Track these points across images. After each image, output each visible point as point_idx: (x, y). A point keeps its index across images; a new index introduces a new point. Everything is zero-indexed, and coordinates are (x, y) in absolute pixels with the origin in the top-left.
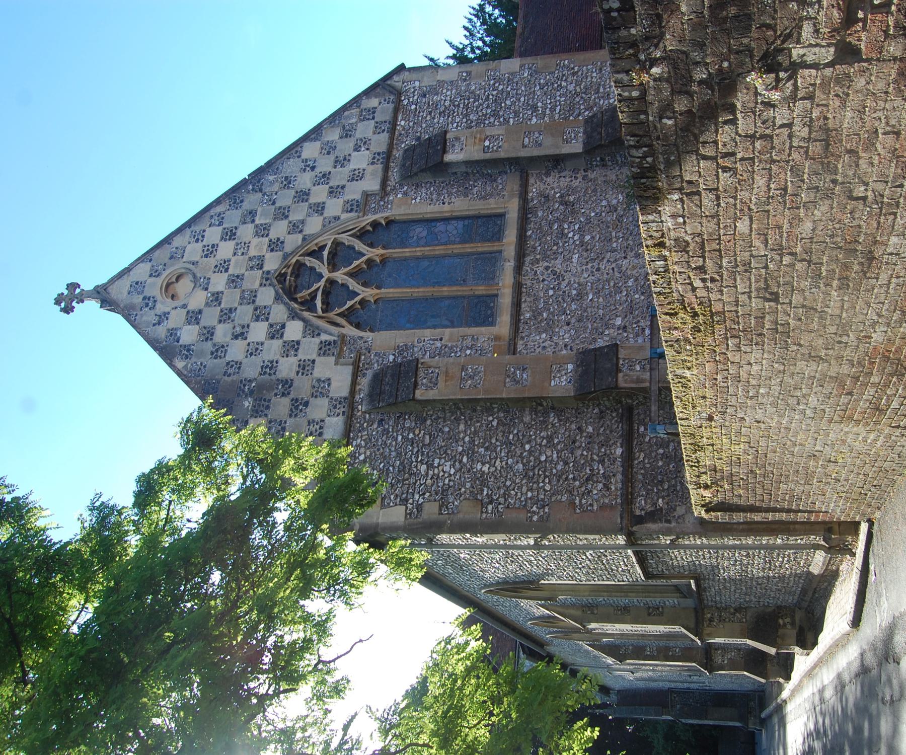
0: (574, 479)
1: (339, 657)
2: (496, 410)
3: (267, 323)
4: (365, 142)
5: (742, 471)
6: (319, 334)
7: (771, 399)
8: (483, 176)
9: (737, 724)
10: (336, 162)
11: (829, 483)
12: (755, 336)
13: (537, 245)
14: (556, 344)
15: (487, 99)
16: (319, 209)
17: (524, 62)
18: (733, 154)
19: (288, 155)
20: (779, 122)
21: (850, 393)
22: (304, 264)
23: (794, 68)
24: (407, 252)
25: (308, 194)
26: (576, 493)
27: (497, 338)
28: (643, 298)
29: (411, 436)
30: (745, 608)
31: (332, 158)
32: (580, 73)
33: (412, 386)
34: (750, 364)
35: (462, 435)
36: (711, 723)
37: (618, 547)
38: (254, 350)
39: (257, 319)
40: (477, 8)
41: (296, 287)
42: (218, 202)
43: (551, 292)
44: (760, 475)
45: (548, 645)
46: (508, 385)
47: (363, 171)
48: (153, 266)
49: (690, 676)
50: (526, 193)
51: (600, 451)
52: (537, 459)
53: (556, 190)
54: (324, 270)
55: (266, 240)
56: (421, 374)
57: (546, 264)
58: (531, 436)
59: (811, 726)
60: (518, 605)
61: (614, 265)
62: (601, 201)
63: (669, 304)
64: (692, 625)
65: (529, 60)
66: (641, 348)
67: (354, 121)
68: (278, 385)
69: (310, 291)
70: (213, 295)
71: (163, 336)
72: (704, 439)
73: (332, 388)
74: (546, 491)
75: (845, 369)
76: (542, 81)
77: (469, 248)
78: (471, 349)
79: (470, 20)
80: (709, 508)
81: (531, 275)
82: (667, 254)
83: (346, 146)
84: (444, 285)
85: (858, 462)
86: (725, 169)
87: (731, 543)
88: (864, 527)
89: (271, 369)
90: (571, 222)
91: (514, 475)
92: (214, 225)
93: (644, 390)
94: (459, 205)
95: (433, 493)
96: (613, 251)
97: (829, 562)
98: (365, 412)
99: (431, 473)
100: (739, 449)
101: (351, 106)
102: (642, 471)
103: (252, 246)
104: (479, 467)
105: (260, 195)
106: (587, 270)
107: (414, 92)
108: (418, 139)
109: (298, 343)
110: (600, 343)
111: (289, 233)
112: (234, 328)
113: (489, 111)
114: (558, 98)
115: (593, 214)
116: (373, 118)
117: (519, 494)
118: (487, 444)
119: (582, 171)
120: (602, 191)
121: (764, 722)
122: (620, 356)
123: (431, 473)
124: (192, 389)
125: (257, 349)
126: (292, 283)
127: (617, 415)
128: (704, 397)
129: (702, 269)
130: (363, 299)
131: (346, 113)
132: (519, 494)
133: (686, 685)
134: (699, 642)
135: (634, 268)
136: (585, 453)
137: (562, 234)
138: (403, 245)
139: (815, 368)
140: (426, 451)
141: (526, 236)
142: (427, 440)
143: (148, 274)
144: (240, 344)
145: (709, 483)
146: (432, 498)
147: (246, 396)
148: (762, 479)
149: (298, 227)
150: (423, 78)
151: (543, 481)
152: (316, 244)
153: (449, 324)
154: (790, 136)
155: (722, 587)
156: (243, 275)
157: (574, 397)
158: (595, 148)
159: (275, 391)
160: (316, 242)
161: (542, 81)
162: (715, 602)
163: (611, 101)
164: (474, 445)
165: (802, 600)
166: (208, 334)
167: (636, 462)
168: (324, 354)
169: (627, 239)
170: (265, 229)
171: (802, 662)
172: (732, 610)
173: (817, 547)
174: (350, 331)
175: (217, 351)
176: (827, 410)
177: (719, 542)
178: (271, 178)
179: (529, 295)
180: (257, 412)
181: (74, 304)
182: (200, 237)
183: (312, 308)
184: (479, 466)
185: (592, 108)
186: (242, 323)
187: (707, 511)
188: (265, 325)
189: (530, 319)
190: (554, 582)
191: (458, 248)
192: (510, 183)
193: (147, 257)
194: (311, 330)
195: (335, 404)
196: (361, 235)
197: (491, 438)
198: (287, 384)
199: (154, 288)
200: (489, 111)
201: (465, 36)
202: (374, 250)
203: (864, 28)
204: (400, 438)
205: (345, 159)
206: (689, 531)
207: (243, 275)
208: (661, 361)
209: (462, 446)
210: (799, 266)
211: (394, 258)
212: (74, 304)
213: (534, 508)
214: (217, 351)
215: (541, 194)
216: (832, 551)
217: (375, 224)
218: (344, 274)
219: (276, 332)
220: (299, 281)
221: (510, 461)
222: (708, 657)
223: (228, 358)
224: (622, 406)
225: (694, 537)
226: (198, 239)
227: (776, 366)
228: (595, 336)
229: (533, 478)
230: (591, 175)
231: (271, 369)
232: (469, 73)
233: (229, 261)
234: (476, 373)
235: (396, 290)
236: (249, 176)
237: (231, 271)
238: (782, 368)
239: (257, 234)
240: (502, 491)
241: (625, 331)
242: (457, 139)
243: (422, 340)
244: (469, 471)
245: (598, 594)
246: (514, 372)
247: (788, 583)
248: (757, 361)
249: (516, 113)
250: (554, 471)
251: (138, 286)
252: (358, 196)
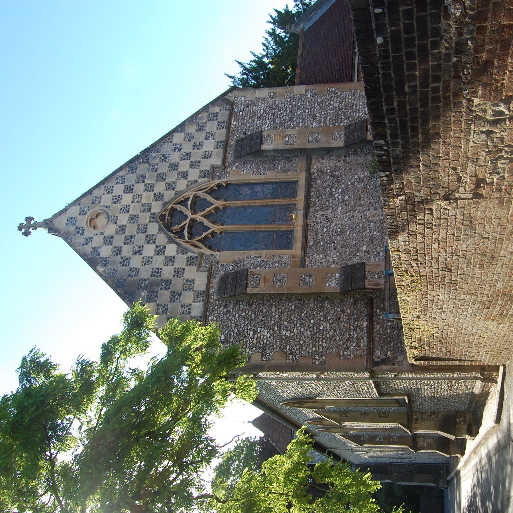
0: (340, 340)
1: (226, 444)
2: (293, 299)
3: (154, 245)
4: (212, 134)
5: (435, 341)
6: (186, 253)
7: (449, 310)
8: (284, 157)
9: (433, 485)
10: (194, 146)
11: (481, 347)
12: (441, 285)
13: (317, 201)
14: (329, 260)
15: (286, 110)
16: (184, 175)
17: (308, 88)
18: (431, 223)
19: (164, 141)
20: (450, 214)
21: (488, 308)
22: (176, 209)
23: (456, 200)
24: (239, 203)
25: (177, 166)
26: (340, 348)
27: (294, 257)
28: (379, 234)
29: (244, 314)
30: (437, 412)
31: (192, 143)
32: (341, 96)
33: (244, 286)
34: (438, 295)
35: (274, 314)
36: (416, 484)
37: (365, 379)
38: (147, 262)
39: (148, 242)
40: (271, 31)
41: (171, 223)
42: (121, 169)
43: (325, 230)
44: (444, 343)
45: (315, 436)
46: (301, 285)
47: (210, 151)
48: (81, 208)
49: (403, 454)
50: (310, 169)
51: (354, 324)
52: (318, 328)
53: (328, 168)
54: (188, 213)
55: (152, 194)
56: (250, 278)
57: (322, 213)
58: (314, 315)
59: (475, 480)
60: (300, 412)
61: (362, 214)
62: (355, 175)
63: (400, 271)
64: (405, 422)
65: (311, 87)
66: (378, 265)
67: (205, 120)
68: (162, 283)
69: (180, 226)
70: (120, 227)
71: (90, 252)
72: (415, 326)
73: (195, 285)
74: (324, 347)
75: (485, 298)
76: (319, 100)
77: (276, 202)
78: (278, 263)
79: (267, 39)
80: (417, 359)
81: (313, 219)
82: (401, 254)
83: (200, 137)
84: (262, 224)
85: (495, 337)
86: (428, 228)
87: (428, 376)
88: (501, 369)
89: (158, 273)
90: (337, 188)
91: (305, 338)
92: (119, 183)
93: (380, 290)
94: (270, 175)
95: (257, 348)
96: (362, 205)
97: (484, 387)
98: (216, 300)
99: (256, 336)
100: (433, 331)
101: (202, 111)
102: (379, 336)
103: (143, 197)
104: (284, 333)
105: (148, 165)
106: (346, 217)
107: (241, 104)
108: (244, 133)
109: (174, 257)
110: (355, 261)
111: (166, 190)
112: (134, 247)
113: (287, 118)
114: (329, 111)
115: (349, 183)
116: (217, 119)
117: (308, 349)
118: (289, 320)
119: (343, 157)
120: (355, 169)
121: (449, 483)
122: (366, 270)
123: (256, 336)
124: (109, 285)
125: (149, 261)
126: (169, 220)
127: (364, 303)
128: (416, 308)
129: (417, 260)
130: (213, 231)
131: (200, 116)
132: (308, 349)
133: (400, 460)
134: (409, 433)
135: (374, 216)
136: (346, 325)
137: (332, 195)
138: (236, 199)
139: (470, 297)
140: (253, 323)
141: (310, 196)
142: (253, 317)
143: (78, 213)
144: (138, 257)
145: (417, 346)
146: (257, 351)
147: (143, 289)
148: (445, 345)
149: (172, 186)
150: (246, 95)
151: (322, 341)
152: (183, 197)
153: (265, 247)
154: (455, 219)
155: (423, 400)
156: (138, 215)
157: (340, 293)
158: (352, 144)
159: (161, 287)
160: (183, 196)
161: (319, 100)
162: (419, 409)
163: (360, 114)
164: (281, 320)
165: (470, 407)
166: (118, 251)
167: (375, 330)
168: (190, 265)
169: (370, 199)
170: (151, 187)
171: (471, 444)
172: (429, 414)
173: (477, 378)
174: (206, 251)
175: (124, 261)
176: (477, 315)
177: (422, 376)
178: (154, 155)
179: (312, 231)
180: (150, 299)
181: (31, 230)
182: (110, 191)
183: (182, 237)
184: (284, 332)
185: (349, 118)
186: (139, 245)
187: (416, 360)
188: (153, 246)
189: (313, 245)
190: (325, 398)
191: (269, 202)
192: (300, 163)
193: (77, 202)
194: (182, 250)
195: (198, 294)
196: (211, 192)
197: (291, 316)
198: (168, 282)
199: (83, 221)
200: (287, 118)
201: (263, 49)
202: (219, 202)
203: (484, 189)
204: (237, 315)
205: (200, 145)
206: (405, 370)
207: (138, 215)
208: (391, 277)
209: (274, 321)
210: (460, 260)
211: (231, 207)
212: (31, 230)
213: (317, 357)
214: (124, 261)
215: (319, 170)
216: (485, 381)
217: (219, 186)
218: (201, 216)
219: (160, 251)
220: (173, 219)
221: (302, 329)
222: (414, 442)
223: (131, 266)
224: (367, 298)
225: (408, 373)
226: (109, 192)
227: (451, 296)
228: (351, 256)
229: (316, 339)
230: (349, 159)
231: (158, 273)
232: (275, 93)
233: (129, 206)
234: (282, 278)
235: (233, 227)
236: (140, 153)
237: (131, 212)
238: (454, 297)
239: (146, 190)
240: (298, 347)
241: (369, 254)
242: (269, 136)
243: (249, 257)
244: (278, 335)
245: (350, 404)
246: (305, 278)
247: (461, 398)
248: (442, 295)
249: (304, 120)
250: (328, 335)
251: (72, 220)
252: (208, 168)
